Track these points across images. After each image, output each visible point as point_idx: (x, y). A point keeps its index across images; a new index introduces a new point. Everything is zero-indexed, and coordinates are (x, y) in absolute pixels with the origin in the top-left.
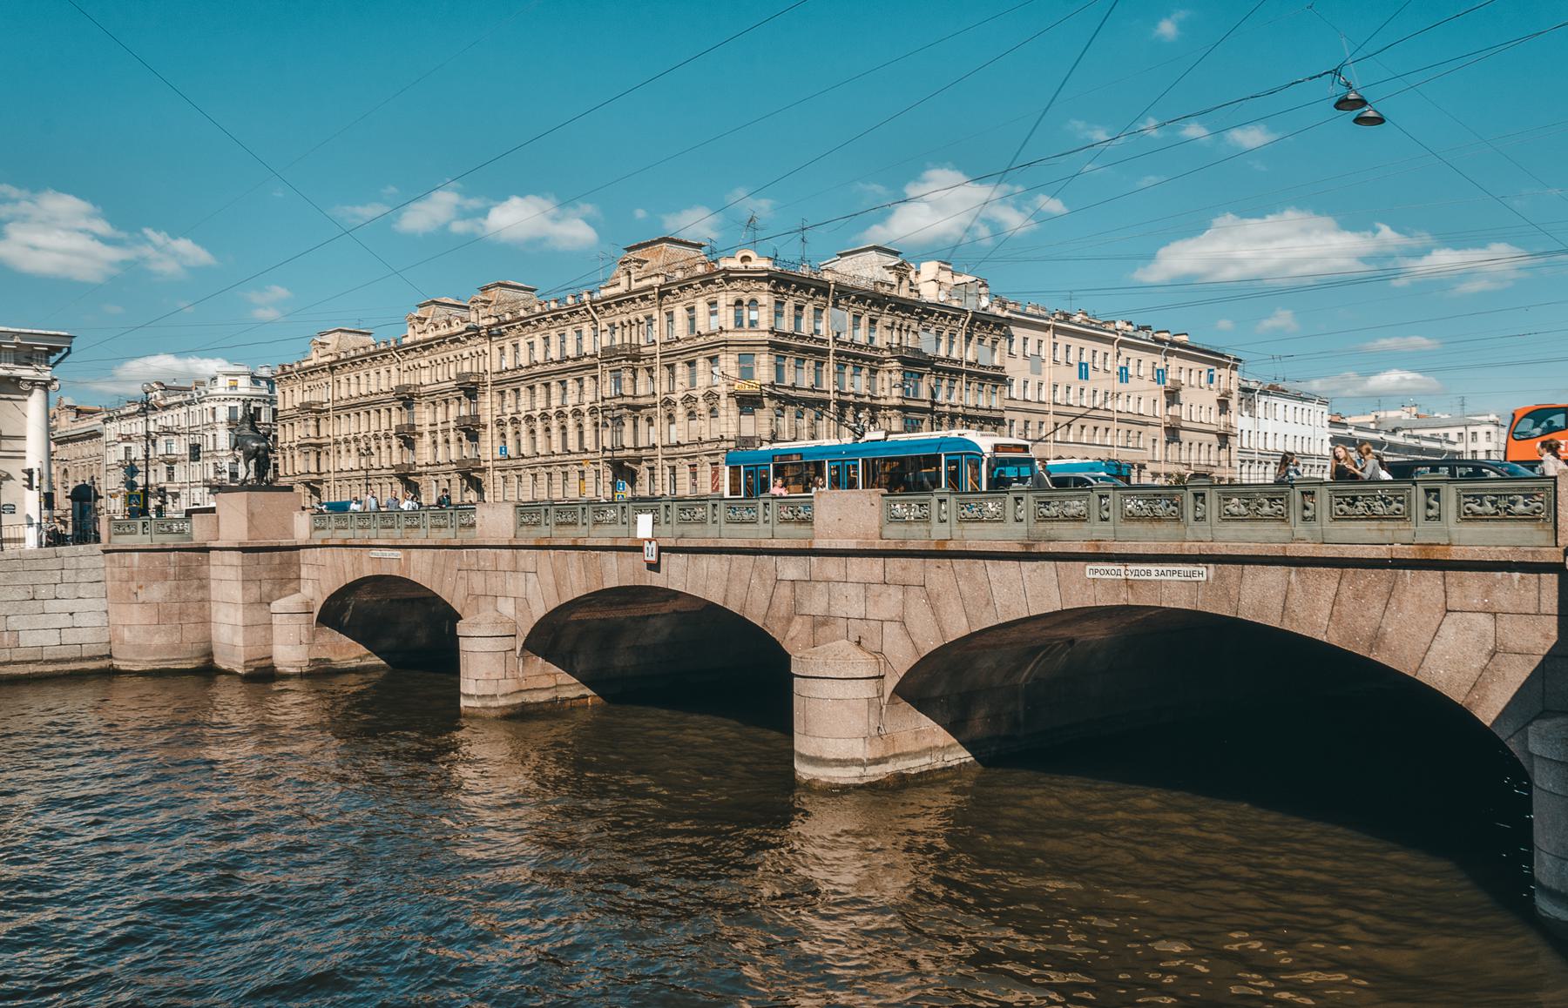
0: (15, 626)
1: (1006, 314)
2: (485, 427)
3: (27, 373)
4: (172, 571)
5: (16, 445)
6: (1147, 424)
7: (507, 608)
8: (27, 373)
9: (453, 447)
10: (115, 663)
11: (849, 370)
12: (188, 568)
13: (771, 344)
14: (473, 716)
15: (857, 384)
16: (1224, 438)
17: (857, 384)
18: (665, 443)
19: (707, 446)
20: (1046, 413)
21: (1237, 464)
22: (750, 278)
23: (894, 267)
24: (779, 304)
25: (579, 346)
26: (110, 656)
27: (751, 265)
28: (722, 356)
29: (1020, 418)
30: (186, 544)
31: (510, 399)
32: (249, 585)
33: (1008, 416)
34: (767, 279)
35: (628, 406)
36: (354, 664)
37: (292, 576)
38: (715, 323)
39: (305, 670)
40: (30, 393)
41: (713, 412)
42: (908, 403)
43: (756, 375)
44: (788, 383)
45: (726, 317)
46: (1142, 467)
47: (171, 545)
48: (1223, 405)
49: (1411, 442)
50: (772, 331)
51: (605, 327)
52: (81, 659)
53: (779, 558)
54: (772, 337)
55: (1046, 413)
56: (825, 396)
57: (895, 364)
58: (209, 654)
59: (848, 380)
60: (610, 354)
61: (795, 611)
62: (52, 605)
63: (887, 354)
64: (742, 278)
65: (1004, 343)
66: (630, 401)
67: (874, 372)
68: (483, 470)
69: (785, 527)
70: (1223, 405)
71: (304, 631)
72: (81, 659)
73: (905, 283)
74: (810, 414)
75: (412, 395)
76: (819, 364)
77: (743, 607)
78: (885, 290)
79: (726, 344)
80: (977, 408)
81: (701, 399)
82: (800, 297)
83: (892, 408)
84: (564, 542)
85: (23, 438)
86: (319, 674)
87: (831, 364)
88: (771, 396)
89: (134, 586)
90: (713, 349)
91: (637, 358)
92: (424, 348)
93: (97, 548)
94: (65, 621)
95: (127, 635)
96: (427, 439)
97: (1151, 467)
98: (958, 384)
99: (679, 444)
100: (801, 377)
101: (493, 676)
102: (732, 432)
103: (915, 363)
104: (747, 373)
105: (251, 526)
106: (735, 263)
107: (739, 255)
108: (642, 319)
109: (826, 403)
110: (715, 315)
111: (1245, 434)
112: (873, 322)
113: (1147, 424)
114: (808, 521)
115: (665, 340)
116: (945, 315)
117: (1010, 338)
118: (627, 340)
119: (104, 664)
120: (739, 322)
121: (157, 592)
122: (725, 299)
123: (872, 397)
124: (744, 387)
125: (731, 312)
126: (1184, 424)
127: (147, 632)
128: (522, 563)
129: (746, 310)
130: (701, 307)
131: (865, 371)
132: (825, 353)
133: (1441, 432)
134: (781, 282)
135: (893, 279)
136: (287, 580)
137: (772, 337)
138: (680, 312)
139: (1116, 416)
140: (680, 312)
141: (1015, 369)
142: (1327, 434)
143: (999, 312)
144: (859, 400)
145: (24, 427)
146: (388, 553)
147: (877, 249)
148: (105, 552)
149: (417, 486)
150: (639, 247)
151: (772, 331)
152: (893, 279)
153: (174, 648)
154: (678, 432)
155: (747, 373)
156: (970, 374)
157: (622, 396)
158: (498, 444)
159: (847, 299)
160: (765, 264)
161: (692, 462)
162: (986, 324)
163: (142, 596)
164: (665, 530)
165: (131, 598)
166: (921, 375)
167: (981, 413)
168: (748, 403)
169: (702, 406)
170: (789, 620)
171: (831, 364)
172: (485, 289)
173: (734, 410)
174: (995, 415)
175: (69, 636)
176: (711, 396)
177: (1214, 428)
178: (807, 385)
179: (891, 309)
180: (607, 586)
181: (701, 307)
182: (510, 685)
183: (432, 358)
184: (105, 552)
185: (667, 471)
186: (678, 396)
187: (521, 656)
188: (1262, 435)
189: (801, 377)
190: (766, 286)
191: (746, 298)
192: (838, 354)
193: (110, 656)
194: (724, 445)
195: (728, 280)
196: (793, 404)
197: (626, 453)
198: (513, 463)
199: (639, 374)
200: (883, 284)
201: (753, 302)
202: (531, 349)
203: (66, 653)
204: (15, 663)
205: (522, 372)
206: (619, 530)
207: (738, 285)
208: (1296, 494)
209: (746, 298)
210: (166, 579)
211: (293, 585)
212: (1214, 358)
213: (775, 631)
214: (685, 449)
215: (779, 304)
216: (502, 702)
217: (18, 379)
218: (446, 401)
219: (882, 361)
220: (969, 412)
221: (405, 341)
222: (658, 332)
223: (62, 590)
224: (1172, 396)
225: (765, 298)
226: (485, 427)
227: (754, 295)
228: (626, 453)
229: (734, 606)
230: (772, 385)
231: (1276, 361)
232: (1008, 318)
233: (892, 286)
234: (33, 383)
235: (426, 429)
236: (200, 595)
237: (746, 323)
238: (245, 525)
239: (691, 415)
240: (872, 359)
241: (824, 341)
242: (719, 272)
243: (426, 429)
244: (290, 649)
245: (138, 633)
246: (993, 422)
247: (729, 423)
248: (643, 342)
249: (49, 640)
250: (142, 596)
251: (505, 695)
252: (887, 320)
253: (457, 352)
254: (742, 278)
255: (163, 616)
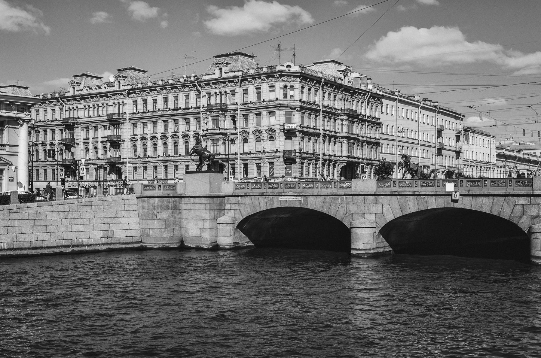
0: (112, 228)
1: (381, 93)
2: (124, 141)
3: (21, 115)
4: (171, 206)
5: (14, 149)
6: (430, 146)
7: (372, 217)
8: (21, 115)
9: (100, 151)
10: (143, 245)
11: (327, 119)
12: (176, 205)
13: (301, 107)
14: (358, 256)
15: (329, 126)
16: (458, 153)
17: (329, 126)
18: (242, 152)
19: (267, 154)
20: (394, 141)
21: (462, 166)
22: (291, 76)
23: (343, 71)
24: (303, 88)
25: (187, 103)
26: (141, 242)
27: (291, 69)
28: (277, 112)
29: (385, 142)
30: (176, 195)
31: (150, 125)
32: (211, 212)
33: (381, 141)
34: (299, 77)
35: (223, 134)
36: (246, 245)
37: (223, 208)
38: (272, 96)
39: (232, 247)
40: (22, 125)
41: (272, 138)
42: (350, 135)
43: (293, 121)
44: (305, 125)
45: (279, 93)
46: (428, 167)
47: (171, 195)
48: (458, 137)
49: (526, 157)
50: (300, 101)
51: (205, 94)
52: (132, 243)
53: (516, 198)
54: (300, 103)
55: (394, 141)
56: (318, 131)
57: (345, 117)
58: (182, 242)
59: (326, 124)
60: (210, 108)
61: (524, 213)
62: (123, 220)
63: (340, 112)
64: (288, 76)
65: (380, 106)
66: (223, 131)
67: (335, 120)
68: (122, 163)
69: (519, 188)
70: (458, 137)
71: (232, 231)
72: (132, 243)
73: (346, 78)
74: (313, 139)
75: (74, 123)
76: (316, 116)
77: (499, 213)
78: (339, 82)
79: (280, 106)
80: (371, 138)
81: (264, 132)
82: (331, 89)
83: (343, 138)
84: (407, 193)
85: (17, 146)
86: (236, 248)
87: (321, 117)
88: (300, 131)
89: (155, 212)
90: (272, 108)
91: (226, 110)
92: (81, 99)
93: (134, 196)
94: (126, 227)
95: (151, 233)
96: (82, 146)
97: (432, 168)
98: (364, 126)
99: (250, 153)
100: (310, 122)
101: (370, 242)
102: (282, 148)
103: (353, 117)
104: (289, 121)
105: (211, 188)
106: (284, 68)
107: (286, 65)
108: (228, 91)
109: (318, 135)
110: (274, 92)
111: (465, 151)
112: (335, 96)
113: (430, 146)
114: (532, 186)
115: (242, 102)
116: (360, 94)
117: (382, 103)
118: (218, 102)
119: (140, 245)
120: (285, 96)
121: (165, 215)
122: (279, 85)
123: (335, 132)
124: (289, 126)
125: (282, 91)
126: (445, 147)
127: (161, 231)
128: (355, 201)
129: (288, 90)
130: (265, 87)
131: (332, 120)
132: (318, 111)
133: (532, 152)
134: (304, 77)
135: (342, 76)
136: (221, 210)
137: (300, 103)
138: (252, 89)
139: (420, 142)
140: (252, 89)
141: (383, 119)
142: (495, 153)
143: (378, 92)
144: (330, 134)
145: (17, 141)
146: (292, 198)
147: (334, 61)
148: (137, 198)
149: (120, 169)
150: (223, 56)
151: (300, 101)
152: (342, 76)
153: (171, 238)
154: (251, 146)
155: (289, 121)
156: (369, 122)
157: (220, 129)
158: (131, 150)
159: (327, 86)
160: (298, 69)
161: (258, 162)
162: (376, 98)
163: (159, 216)
164: (461, 189)
165: (154, 217)
166: (354, 122)
167: (372, 140)
168: (289, 134)
169: (265, 135)
170: (521, 217)
171: (321, 117)
172: (121, 70)
173: (283, 137)
174: (377, 141)
175: (129, 233)
176: (271, 130)
177: (454, 149)
178: (312, 126)
179: (342, 91)
180: (429, 208)
181: (265, 87)
182: (374, 245)
183: (86, 104)
184: (137, 198)
185: (242, 166)
186: (250, 130)
187: (378, 235)
188: (471, 153)
189: (310, 122)
190: (298, 80)
191: (289, 85)
192: (323, 112)
193: (141, 242)
194: (278, 154)
195: (281, 76)
196: (307, 135)
197: (221, 157)
198: (141, 160)
199: (227, 118)
200: (339, 79)
201: (292, 87)
202: (156, 102)
203: (128, 240)
204: (113, 244)
205: (149, 114)
206: (437, 189)
207: (285, 78)
208: (333, 183)
209: (289, 85)
210: (168, 209)
211: (223, 212)
212: (457, 116)
213: (515, 221)
214: (254, 156)
215: (303, 88)
216: (372, 251)
217: (19, 118)
218: (95, 127)
219: (338, 115)
220: (369, 140)
221: (67, 95)
222: (239, 98)
223: (126, 214)
224: (440, 133)
225: (297, 85)
226: (124, 141)
227: (292, 83)
228: (221, 157)
229: (495, 213)
230: (300, 126)
231: (465, 117)
232: (383, 95)
233: (342, 80)
234: (24, 120)
235: (81, 141)
236: (179, 216)
237: (288, 97)
238: (208, 186)
239: (258, 140)
240: (335, 114)
241: (318, 105)
242: (277, 72)
243: (81, 141)
244: (226, 240)
245: (157, 233)
246: (375, 144)
247: (281, 144)
248: (228, 102)
249: (122, 234)
250: (159, 216)
251: (373, 249)
252: (340, 96)
253: (105, 102)
254: (288, 76)
255: (167, 224)
